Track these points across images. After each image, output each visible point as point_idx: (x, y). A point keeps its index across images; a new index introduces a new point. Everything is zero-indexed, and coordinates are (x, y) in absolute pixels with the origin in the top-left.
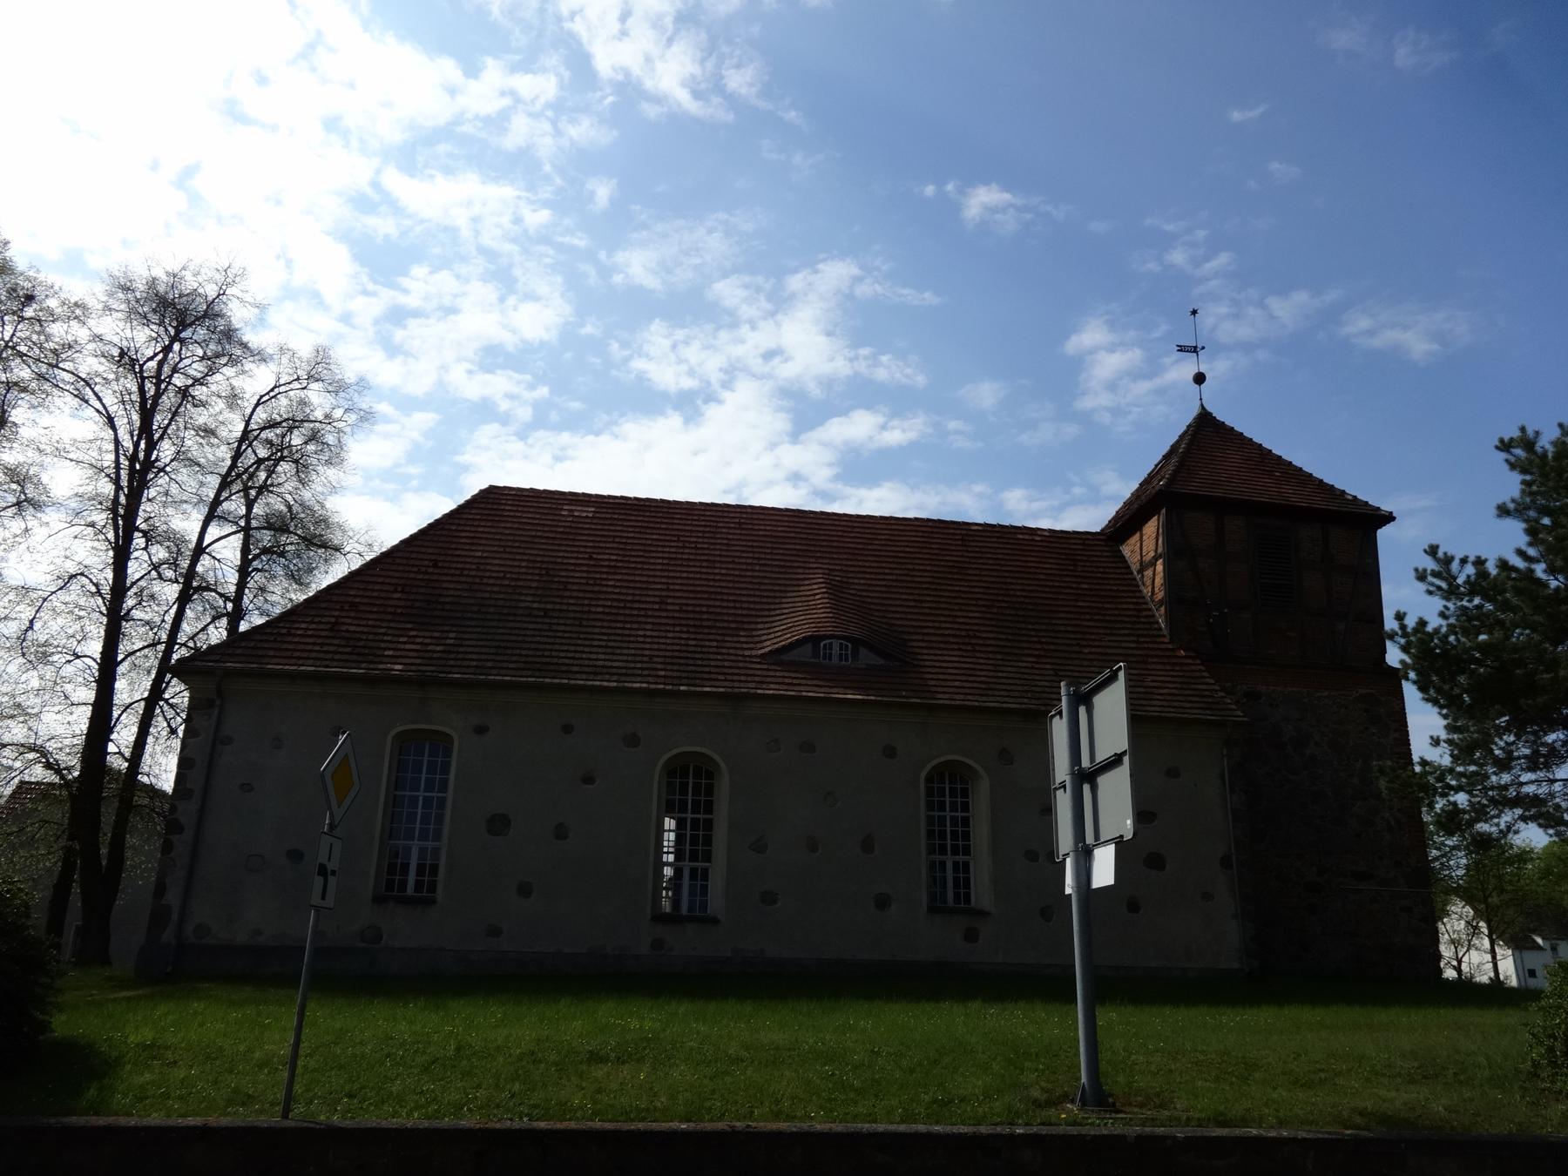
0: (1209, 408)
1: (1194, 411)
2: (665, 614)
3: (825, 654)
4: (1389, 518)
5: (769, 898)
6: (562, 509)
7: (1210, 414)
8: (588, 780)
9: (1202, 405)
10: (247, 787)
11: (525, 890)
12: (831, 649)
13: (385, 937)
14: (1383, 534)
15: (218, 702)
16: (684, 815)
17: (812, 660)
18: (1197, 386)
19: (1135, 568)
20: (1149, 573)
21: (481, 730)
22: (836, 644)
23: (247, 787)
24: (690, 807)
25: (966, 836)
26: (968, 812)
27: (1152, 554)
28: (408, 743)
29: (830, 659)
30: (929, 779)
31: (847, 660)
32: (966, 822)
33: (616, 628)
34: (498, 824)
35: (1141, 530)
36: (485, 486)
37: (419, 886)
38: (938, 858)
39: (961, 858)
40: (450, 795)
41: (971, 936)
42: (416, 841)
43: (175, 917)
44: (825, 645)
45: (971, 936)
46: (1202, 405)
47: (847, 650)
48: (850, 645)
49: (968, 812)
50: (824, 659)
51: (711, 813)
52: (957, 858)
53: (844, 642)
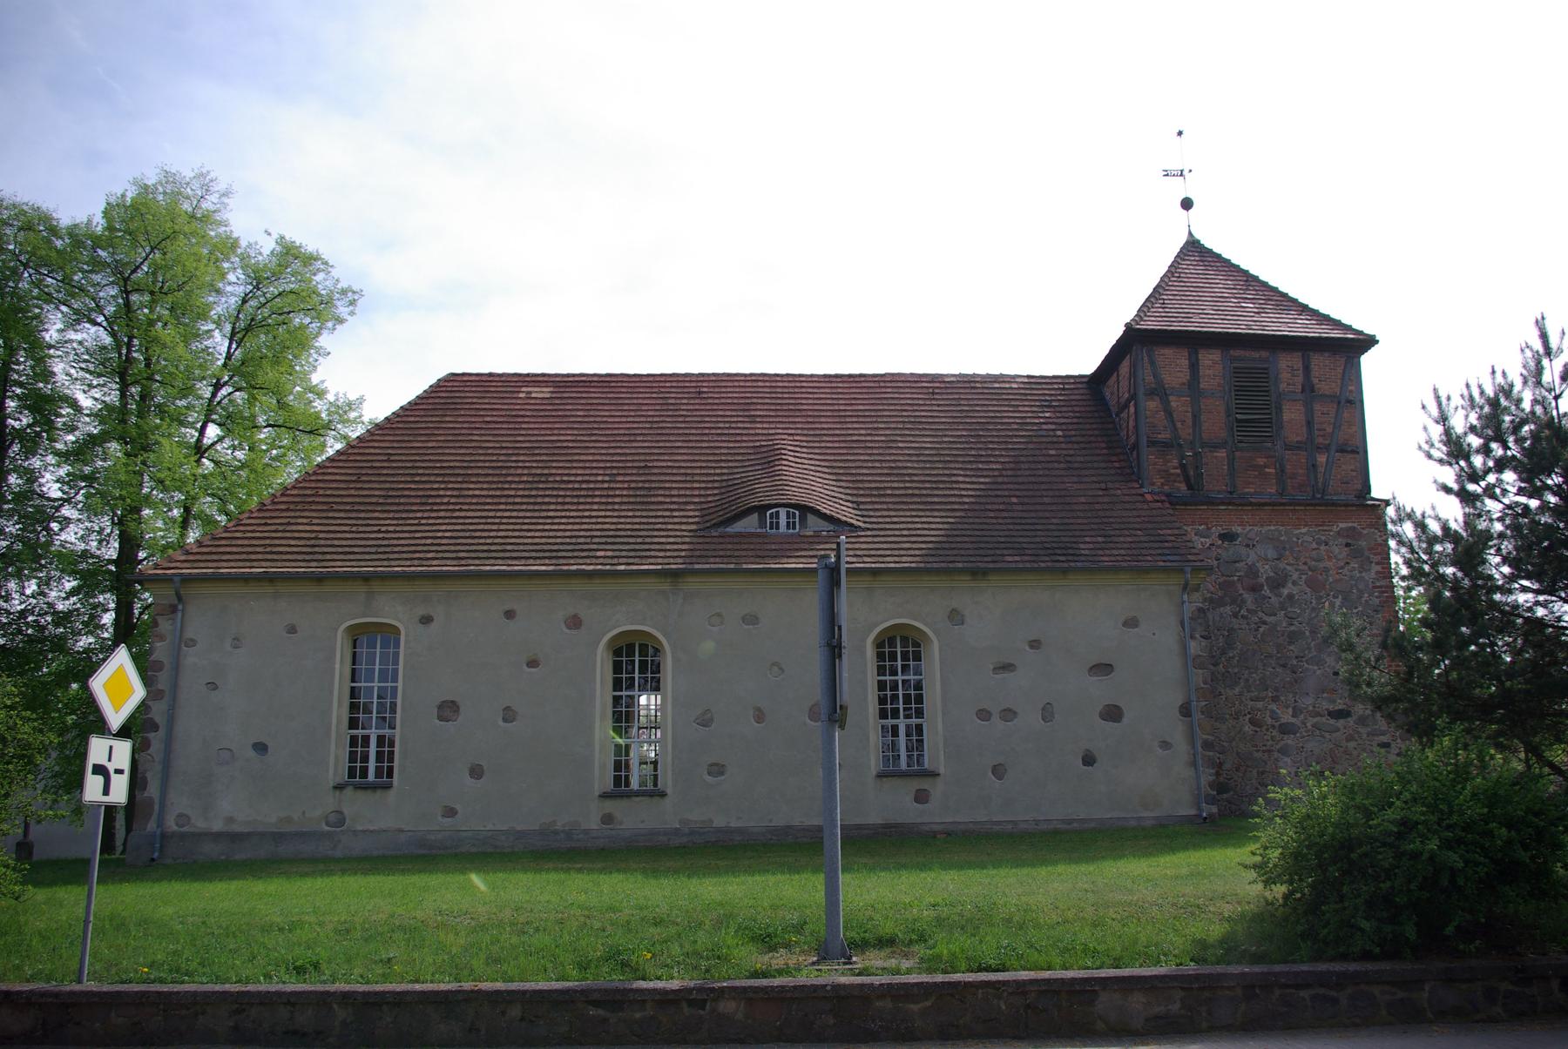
0: (1197, 235)
1: (1183, 239)
2: (1013, 403)
3: (771, 523)
4: (1368, 342)
5: (717, 769)
6: (519, 392)
7: (1198, 241)
8: (533, 663)
9: (1190, 233)
10: (212, 686)
11: (476, 772)
12: (778, 517)
13: (347, 821)
14: (1367, 361)
15: (180, 607)
16: (631, 693)
17: (759, 530)
18: (1185, 211)
19: (1114, 410)
20: (1124, 415)
21: (426, 620)
22: (783, 512)
23: (212, 686)
24: (374, 725)
25: (919, 699)
26: (879, 681)
27: (1126, 395)
28: (357, 635)
29: (778, 528)
30: (879, 644)
31: (794, 528)
32: (918, 686)
33: (549, 510)
34: (448, 709)
35: (1117, 370)
36: (442, 373)
37: (379, 772)
38: (890, 722)
39: (914, 721)
40: (400, 685)
41: (921, 797)
42: (373, 730)
43: (156, 807)
44: (771, 514)
45: (921, 797)
46: (1190, 233)
47: (794, 517)
48: (797, 512)
49: (879, 681)
50: (771, 528)
51: (614, 697)
52: (909, 721)
53: (791, 510)
